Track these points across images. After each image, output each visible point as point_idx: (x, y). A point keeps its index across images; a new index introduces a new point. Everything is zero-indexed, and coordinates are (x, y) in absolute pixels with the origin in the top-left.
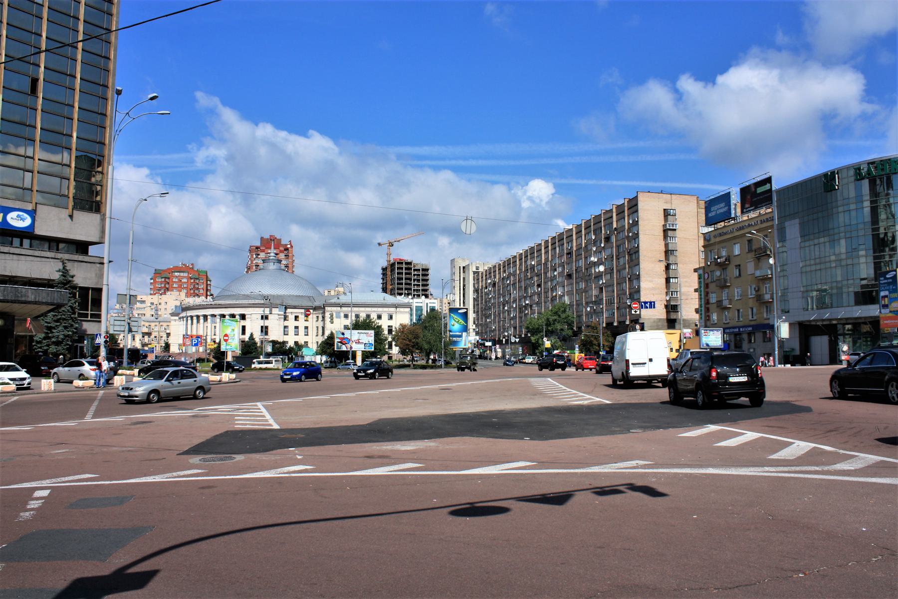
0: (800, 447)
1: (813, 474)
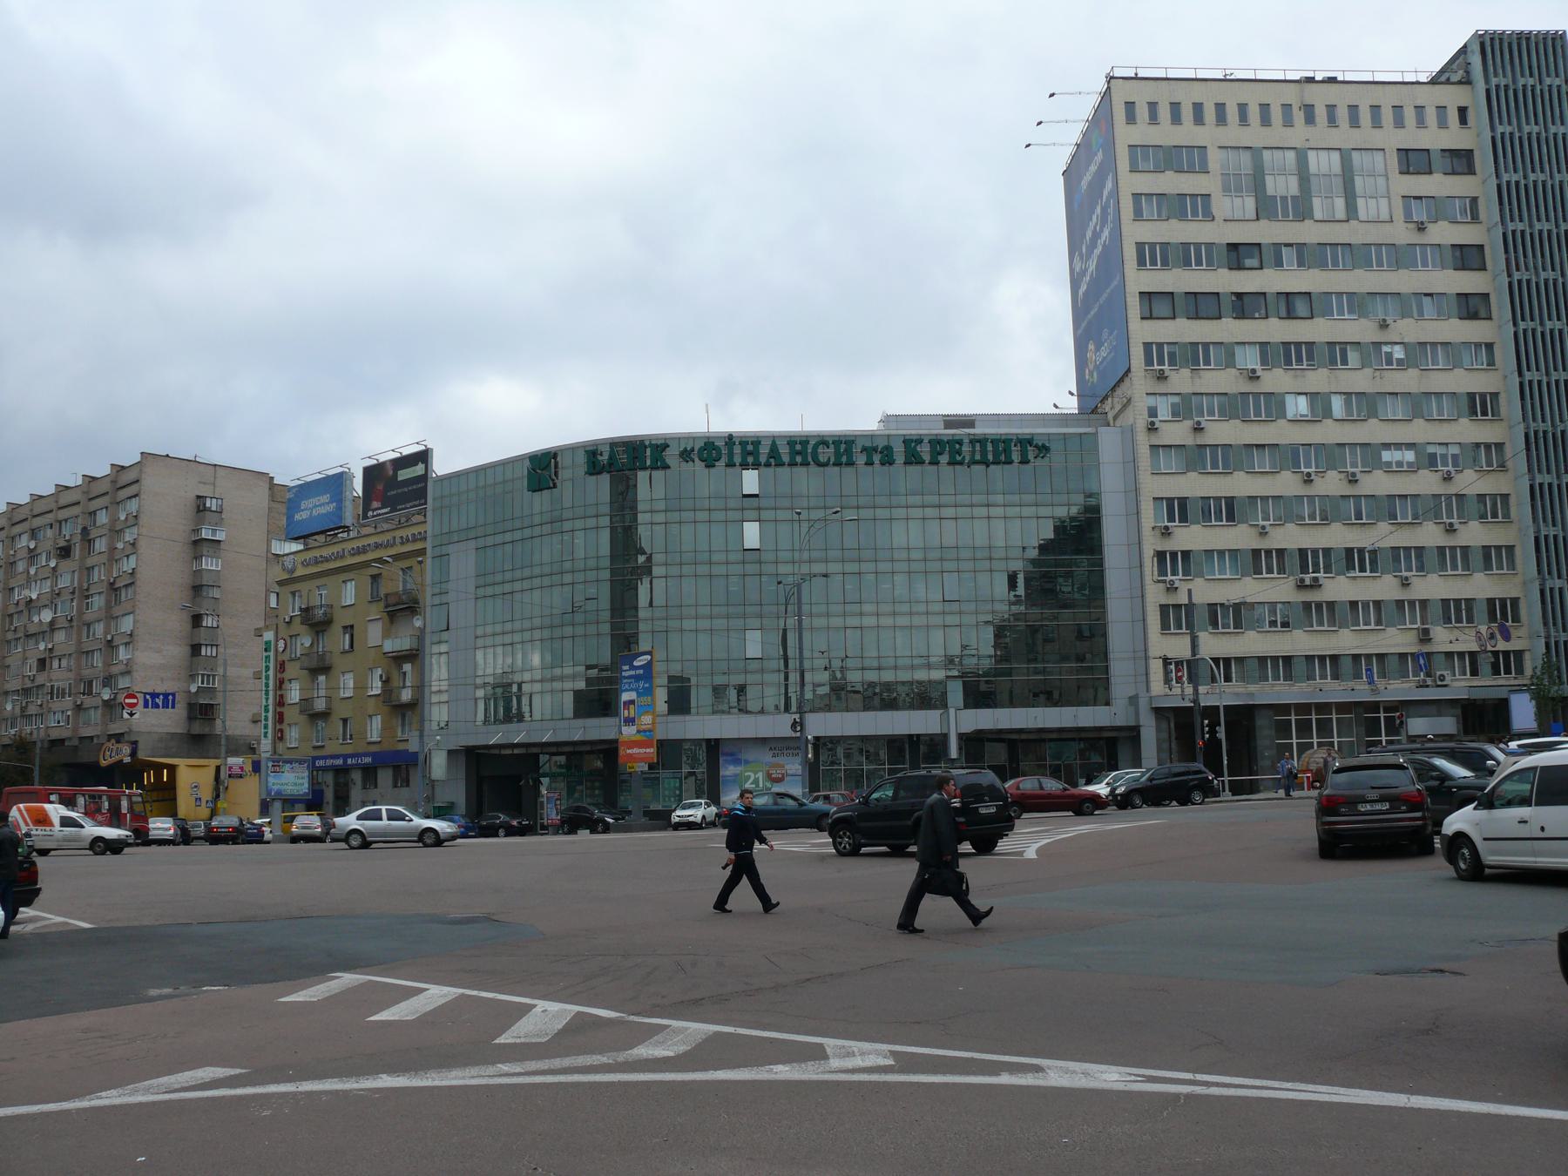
0: (546, 1015)
1: (585, 1070)
